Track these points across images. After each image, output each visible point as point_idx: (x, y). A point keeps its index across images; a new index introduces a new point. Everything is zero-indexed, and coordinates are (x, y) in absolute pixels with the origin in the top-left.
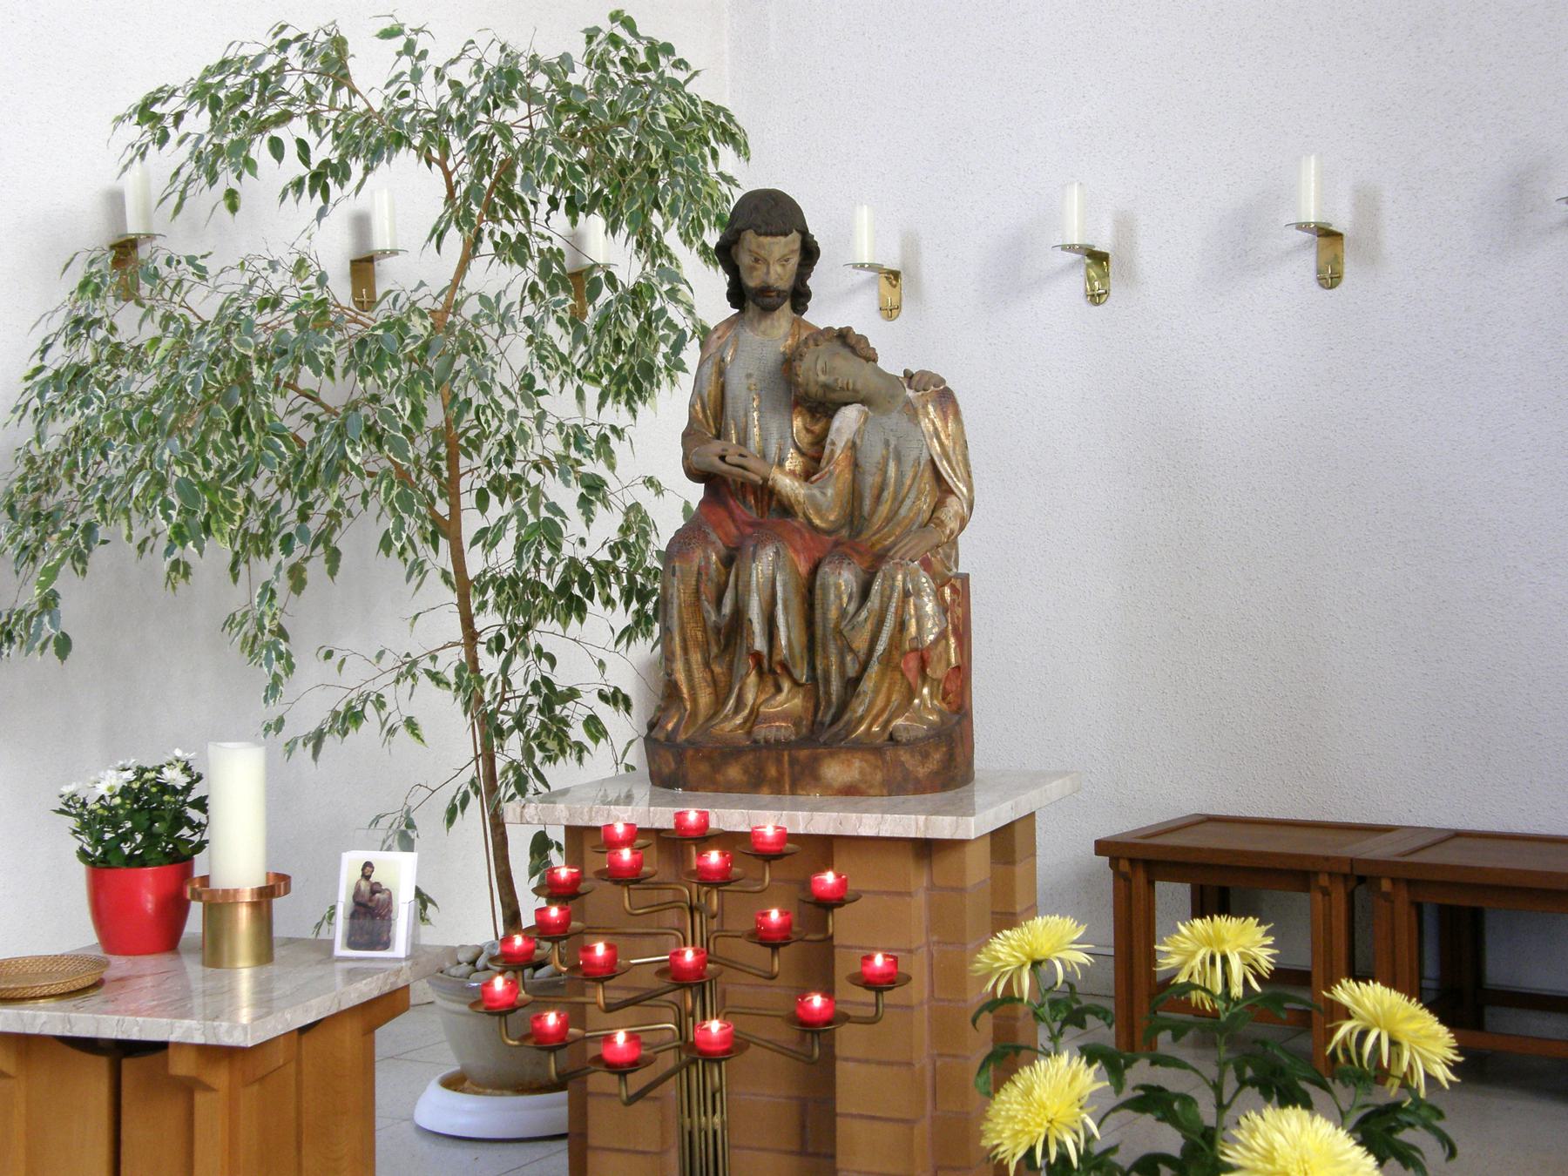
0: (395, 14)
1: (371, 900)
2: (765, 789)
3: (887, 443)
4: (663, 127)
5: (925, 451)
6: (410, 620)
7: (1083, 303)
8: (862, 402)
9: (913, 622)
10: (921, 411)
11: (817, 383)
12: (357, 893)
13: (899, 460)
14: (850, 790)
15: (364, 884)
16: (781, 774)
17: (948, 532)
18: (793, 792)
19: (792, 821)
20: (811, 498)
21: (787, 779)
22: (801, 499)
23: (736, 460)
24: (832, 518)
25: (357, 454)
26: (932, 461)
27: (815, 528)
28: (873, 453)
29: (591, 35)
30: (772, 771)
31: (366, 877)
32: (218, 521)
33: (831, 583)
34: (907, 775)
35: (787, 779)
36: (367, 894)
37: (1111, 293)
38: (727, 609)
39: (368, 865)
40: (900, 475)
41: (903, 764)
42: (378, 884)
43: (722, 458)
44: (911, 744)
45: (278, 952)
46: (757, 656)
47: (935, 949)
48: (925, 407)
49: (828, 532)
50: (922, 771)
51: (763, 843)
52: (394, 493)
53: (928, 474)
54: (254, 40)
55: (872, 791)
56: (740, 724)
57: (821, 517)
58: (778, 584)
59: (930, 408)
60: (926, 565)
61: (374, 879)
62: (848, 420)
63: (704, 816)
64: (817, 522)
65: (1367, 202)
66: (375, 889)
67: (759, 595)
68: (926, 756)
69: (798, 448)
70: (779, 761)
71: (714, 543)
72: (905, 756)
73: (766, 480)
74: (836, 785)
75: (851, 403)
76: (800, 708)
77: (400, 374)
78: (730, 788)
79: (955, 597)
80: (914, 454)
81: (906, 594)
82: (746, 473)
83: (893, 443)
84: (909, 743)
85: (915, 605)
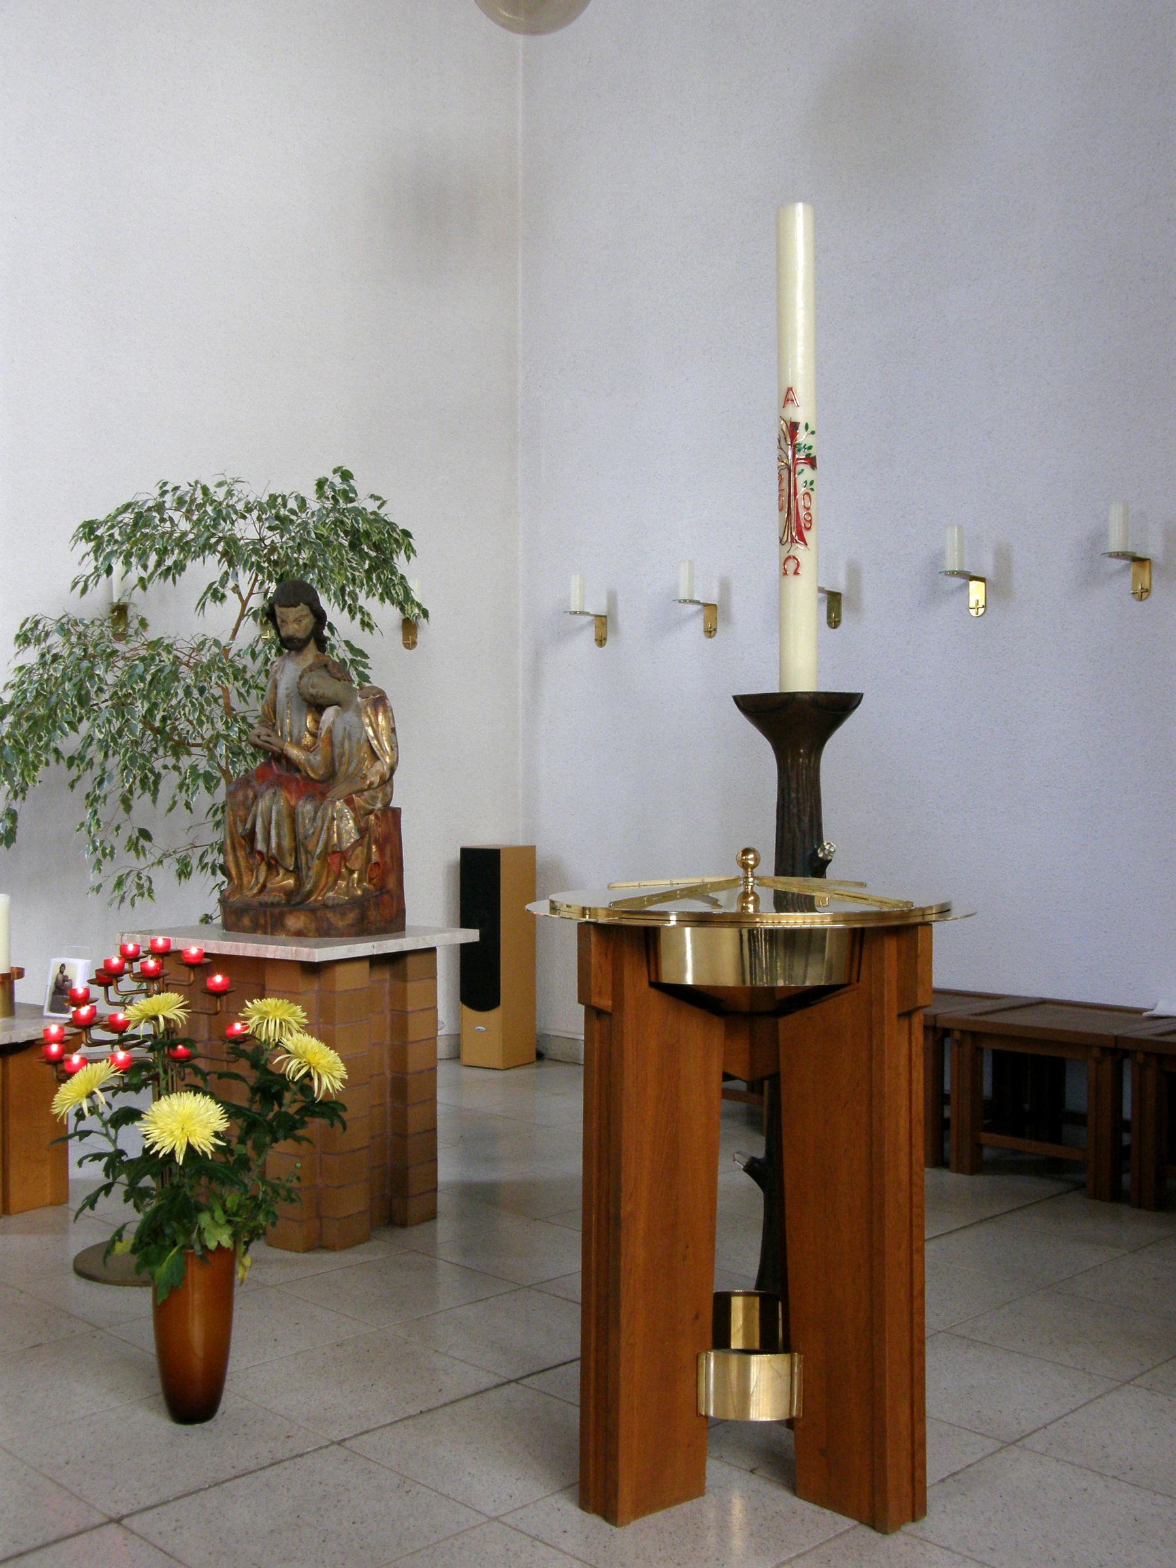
0: (226, 473)
1: (63, 985)
2: (259, 931)
3: (345, 729)
4: (313, 539)
5: (364, 734)
6: (186, 831)
7: (594, 644)
8: (338, 704)
9: (335, 835)
10: (363, 711)
11: (308, 693)
12: (57, 982)
13: (350, 739)
14: (299, 934)
15: (60, 976)
16: (266, 924)
17: (368, 782)
18: (272, 934)
19: (237, 948)
20: (308, 761)
21: (269, 925)
22: (302, 761)
23: (265, 738)
24: (321, 772)
25: (102, 733)
26: (369, 741)
27: (312, 779)
28: (338, 735)
29: (321, 484)
30: (262, 921)
31: (61, 972)
32: (29, 770)
33: (300, 811)
34: (330, 926)
35: (269, 925)
36: (62, 982)
37: (718, 630)
38: (248, 826)
39: (63, 965)
40: (351, 748)
41: (328, 919)
42: (67, 976)
43: (259, 737)
44: (333, 908)
45: (18, 1011)
46: (260, 853)
47: (321, 1026)
48: (365, 708)
49: (319, 782)
50: (341, 924)
51: (188, 958)
52: (128, 755)
53: (365, 748)
54: (148, 495)
55: (311, 934)
56: (256, 894)
57: (314, 772)
58: (273, 812)
59: (369, 709)
60: (349, 802)
61: (65, 974)
62: (329, 714)
63: (168, 942)
64: (312, 775)
65: (854, 573)
66: (65, 979)
67: (263, 818)
68: (343, 915)
69: (309, 731)
70: (265, 915)
71: (254, 787)
72: (330, 915)
73: (282, 750)
74: (292, 930)
75: (332, 705)
76: (293, 885)
77: (145, 686)
78: (243, 930)
79: (377, 821)
80: (358, 735)
81: (333, 819)
82: (271, 746)
83: (348, 729)
84: (333, 907)
85: (338, 826)
